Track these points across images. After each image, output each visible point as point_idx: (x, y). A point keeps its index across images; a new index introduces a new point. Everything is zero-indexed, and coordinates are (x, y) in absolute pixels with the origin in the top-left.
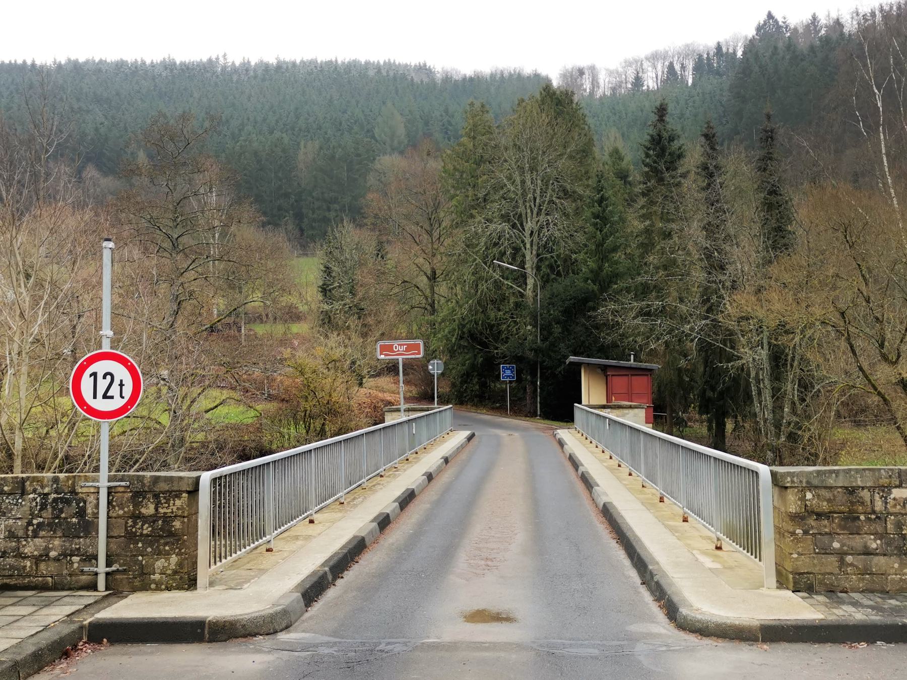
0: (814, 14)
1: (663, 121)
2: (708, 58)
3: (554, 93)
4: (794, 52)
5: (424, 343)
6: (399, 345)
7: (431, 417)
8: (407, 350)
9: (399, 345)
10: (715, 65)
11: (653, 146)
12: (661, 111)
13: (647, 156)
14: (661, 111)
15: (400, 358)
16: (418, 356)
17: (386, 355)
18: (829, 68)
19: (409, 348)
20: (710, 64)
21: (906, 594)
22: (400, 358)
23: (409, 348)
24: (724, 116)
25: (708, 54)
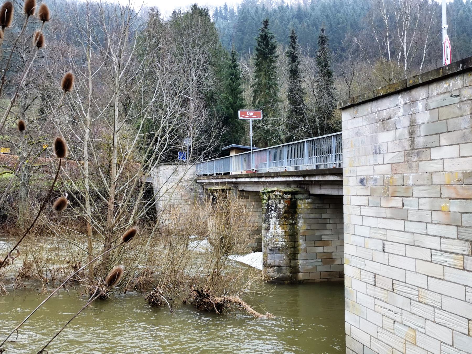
0: (226, 3)
1: (267, 28)
2: (220, 11)
3: (199, 9)
4: (267, 11)
5: (263, 112)
6: (250, 112)
7: (280, 149)
8: (254, 115)
9: (250, 112)
10: (224, 14)
11: (262, 41)
12: (266, 23)
13: (259, 45)
14: (266, 23)
15: (251, 119)
16: (259, 118)
17: (243, 117)
18: (284, 22)
19: (255, 114)
20: (221, 13)
21: (1, 325)
22: (251, 119)
23: (255, 114)
24: (230, 41)
25: (220, 8)
